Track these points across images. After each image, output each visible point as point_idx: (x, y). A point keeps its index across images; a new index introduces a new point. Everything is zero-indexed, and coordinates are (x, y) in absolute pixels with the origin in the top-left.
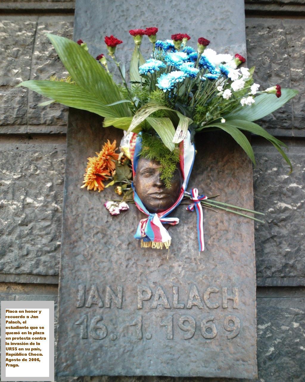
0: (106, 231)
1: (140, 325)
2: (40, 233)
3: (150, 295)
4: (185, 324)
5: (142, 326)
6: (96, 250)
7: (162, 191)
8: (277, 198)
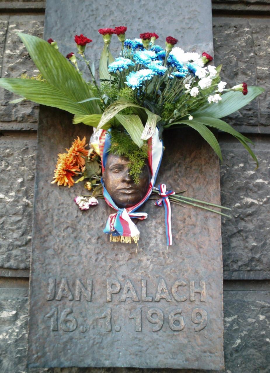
0: (76, 226)
3: (119, 288)
4: (153, 316)
7: (131, 186)
8: (244, 194)
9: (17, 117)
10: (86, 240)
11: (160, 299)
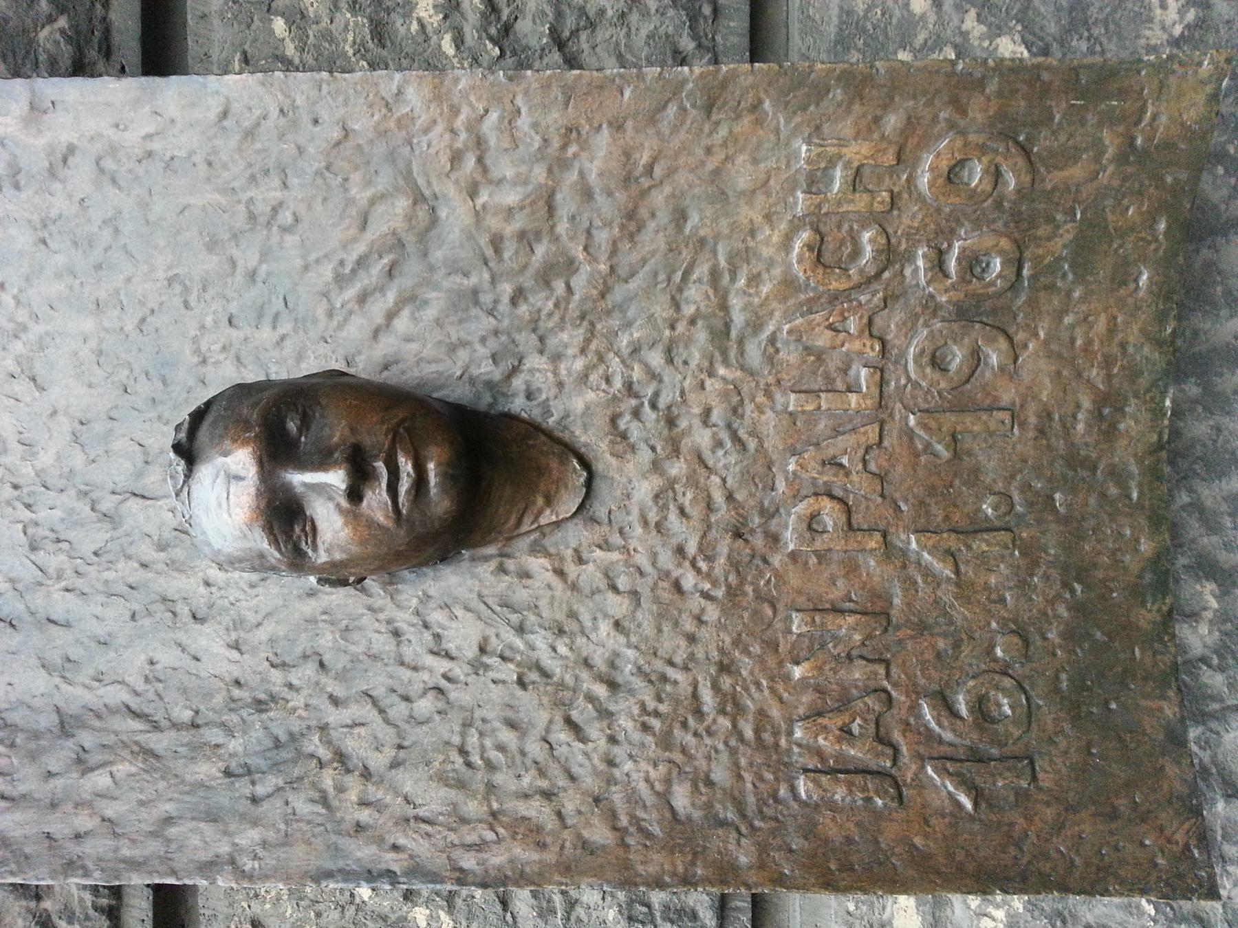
2: (559, 915)
8: (399, 21)
9: (96, 908)
10: (622, 639)
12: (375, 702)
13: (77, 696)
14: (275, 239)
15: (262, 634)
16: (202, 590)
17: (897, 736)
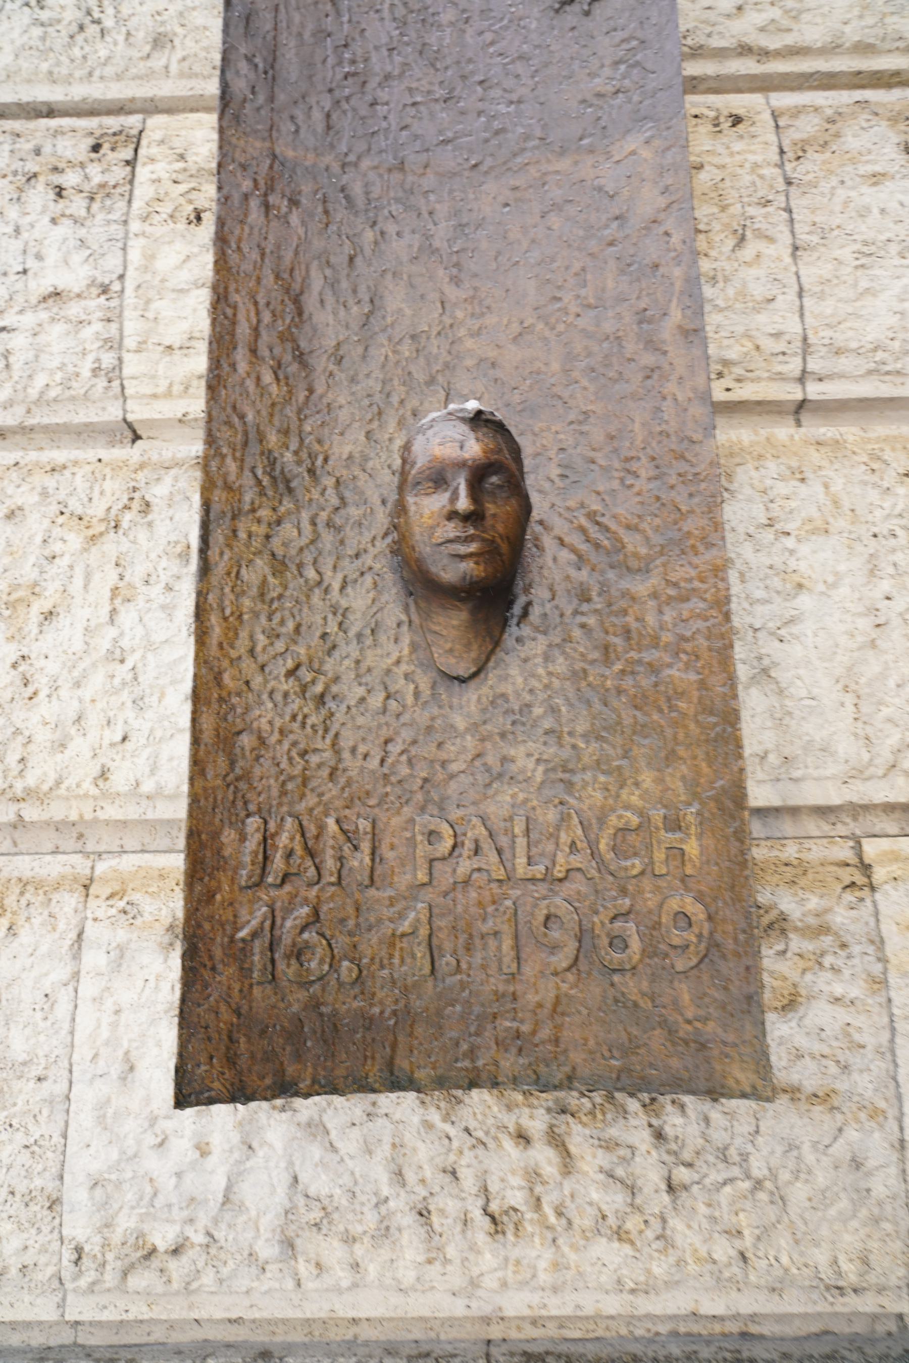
0: (322, 662)
1: (423, 932)
3: (449, 843)
4: (549, 925)
5: (430, 936)
6: (294, 717)
7: (472, 531)
10: (353, 703)
11: (568, 871)
12: (312, 542)
13: (321, 363)
14: (616, 474)
15: (357, 472)
16: (387, 436)
17: (287, 888)
